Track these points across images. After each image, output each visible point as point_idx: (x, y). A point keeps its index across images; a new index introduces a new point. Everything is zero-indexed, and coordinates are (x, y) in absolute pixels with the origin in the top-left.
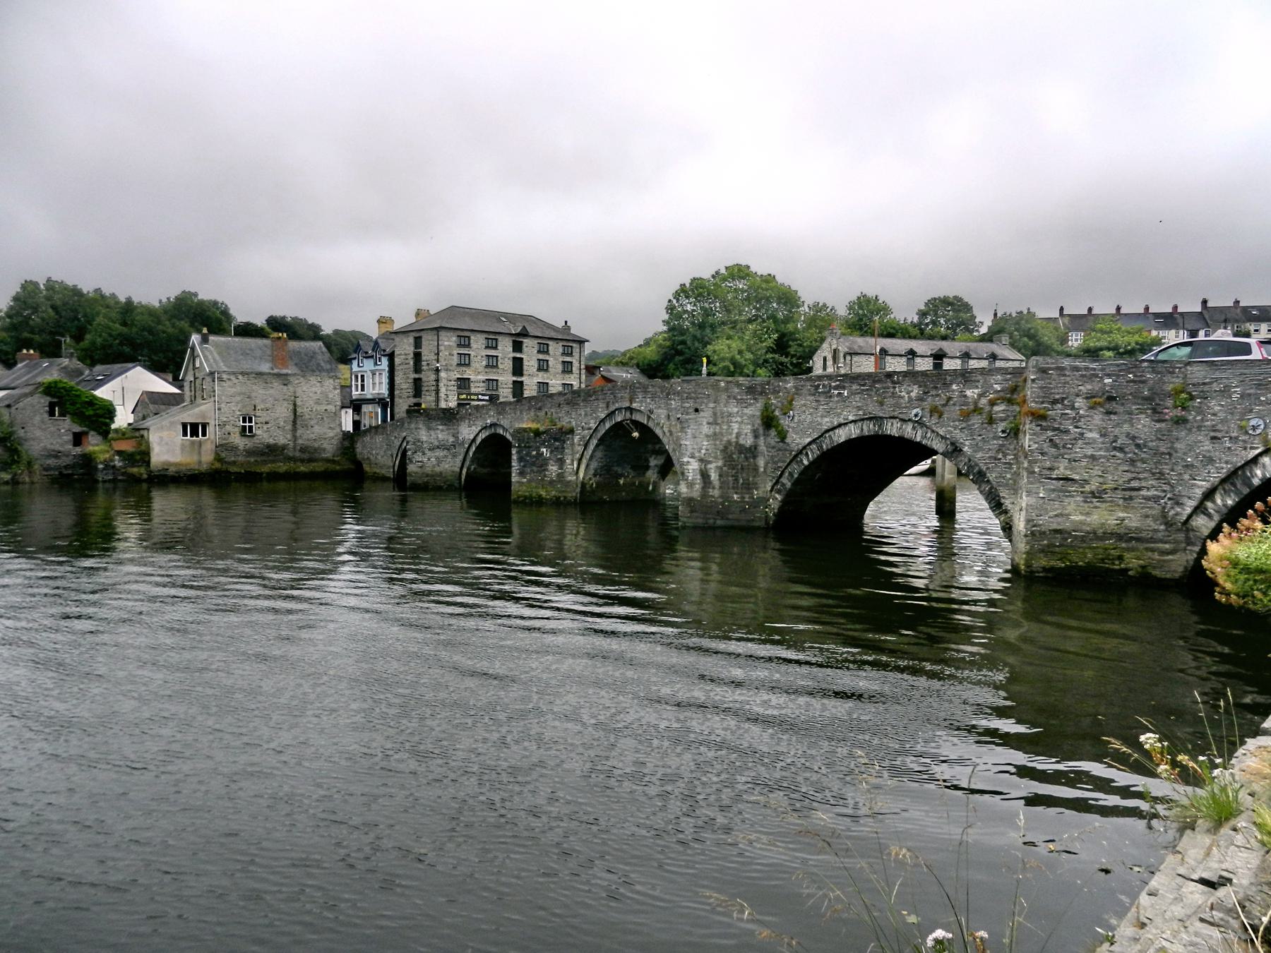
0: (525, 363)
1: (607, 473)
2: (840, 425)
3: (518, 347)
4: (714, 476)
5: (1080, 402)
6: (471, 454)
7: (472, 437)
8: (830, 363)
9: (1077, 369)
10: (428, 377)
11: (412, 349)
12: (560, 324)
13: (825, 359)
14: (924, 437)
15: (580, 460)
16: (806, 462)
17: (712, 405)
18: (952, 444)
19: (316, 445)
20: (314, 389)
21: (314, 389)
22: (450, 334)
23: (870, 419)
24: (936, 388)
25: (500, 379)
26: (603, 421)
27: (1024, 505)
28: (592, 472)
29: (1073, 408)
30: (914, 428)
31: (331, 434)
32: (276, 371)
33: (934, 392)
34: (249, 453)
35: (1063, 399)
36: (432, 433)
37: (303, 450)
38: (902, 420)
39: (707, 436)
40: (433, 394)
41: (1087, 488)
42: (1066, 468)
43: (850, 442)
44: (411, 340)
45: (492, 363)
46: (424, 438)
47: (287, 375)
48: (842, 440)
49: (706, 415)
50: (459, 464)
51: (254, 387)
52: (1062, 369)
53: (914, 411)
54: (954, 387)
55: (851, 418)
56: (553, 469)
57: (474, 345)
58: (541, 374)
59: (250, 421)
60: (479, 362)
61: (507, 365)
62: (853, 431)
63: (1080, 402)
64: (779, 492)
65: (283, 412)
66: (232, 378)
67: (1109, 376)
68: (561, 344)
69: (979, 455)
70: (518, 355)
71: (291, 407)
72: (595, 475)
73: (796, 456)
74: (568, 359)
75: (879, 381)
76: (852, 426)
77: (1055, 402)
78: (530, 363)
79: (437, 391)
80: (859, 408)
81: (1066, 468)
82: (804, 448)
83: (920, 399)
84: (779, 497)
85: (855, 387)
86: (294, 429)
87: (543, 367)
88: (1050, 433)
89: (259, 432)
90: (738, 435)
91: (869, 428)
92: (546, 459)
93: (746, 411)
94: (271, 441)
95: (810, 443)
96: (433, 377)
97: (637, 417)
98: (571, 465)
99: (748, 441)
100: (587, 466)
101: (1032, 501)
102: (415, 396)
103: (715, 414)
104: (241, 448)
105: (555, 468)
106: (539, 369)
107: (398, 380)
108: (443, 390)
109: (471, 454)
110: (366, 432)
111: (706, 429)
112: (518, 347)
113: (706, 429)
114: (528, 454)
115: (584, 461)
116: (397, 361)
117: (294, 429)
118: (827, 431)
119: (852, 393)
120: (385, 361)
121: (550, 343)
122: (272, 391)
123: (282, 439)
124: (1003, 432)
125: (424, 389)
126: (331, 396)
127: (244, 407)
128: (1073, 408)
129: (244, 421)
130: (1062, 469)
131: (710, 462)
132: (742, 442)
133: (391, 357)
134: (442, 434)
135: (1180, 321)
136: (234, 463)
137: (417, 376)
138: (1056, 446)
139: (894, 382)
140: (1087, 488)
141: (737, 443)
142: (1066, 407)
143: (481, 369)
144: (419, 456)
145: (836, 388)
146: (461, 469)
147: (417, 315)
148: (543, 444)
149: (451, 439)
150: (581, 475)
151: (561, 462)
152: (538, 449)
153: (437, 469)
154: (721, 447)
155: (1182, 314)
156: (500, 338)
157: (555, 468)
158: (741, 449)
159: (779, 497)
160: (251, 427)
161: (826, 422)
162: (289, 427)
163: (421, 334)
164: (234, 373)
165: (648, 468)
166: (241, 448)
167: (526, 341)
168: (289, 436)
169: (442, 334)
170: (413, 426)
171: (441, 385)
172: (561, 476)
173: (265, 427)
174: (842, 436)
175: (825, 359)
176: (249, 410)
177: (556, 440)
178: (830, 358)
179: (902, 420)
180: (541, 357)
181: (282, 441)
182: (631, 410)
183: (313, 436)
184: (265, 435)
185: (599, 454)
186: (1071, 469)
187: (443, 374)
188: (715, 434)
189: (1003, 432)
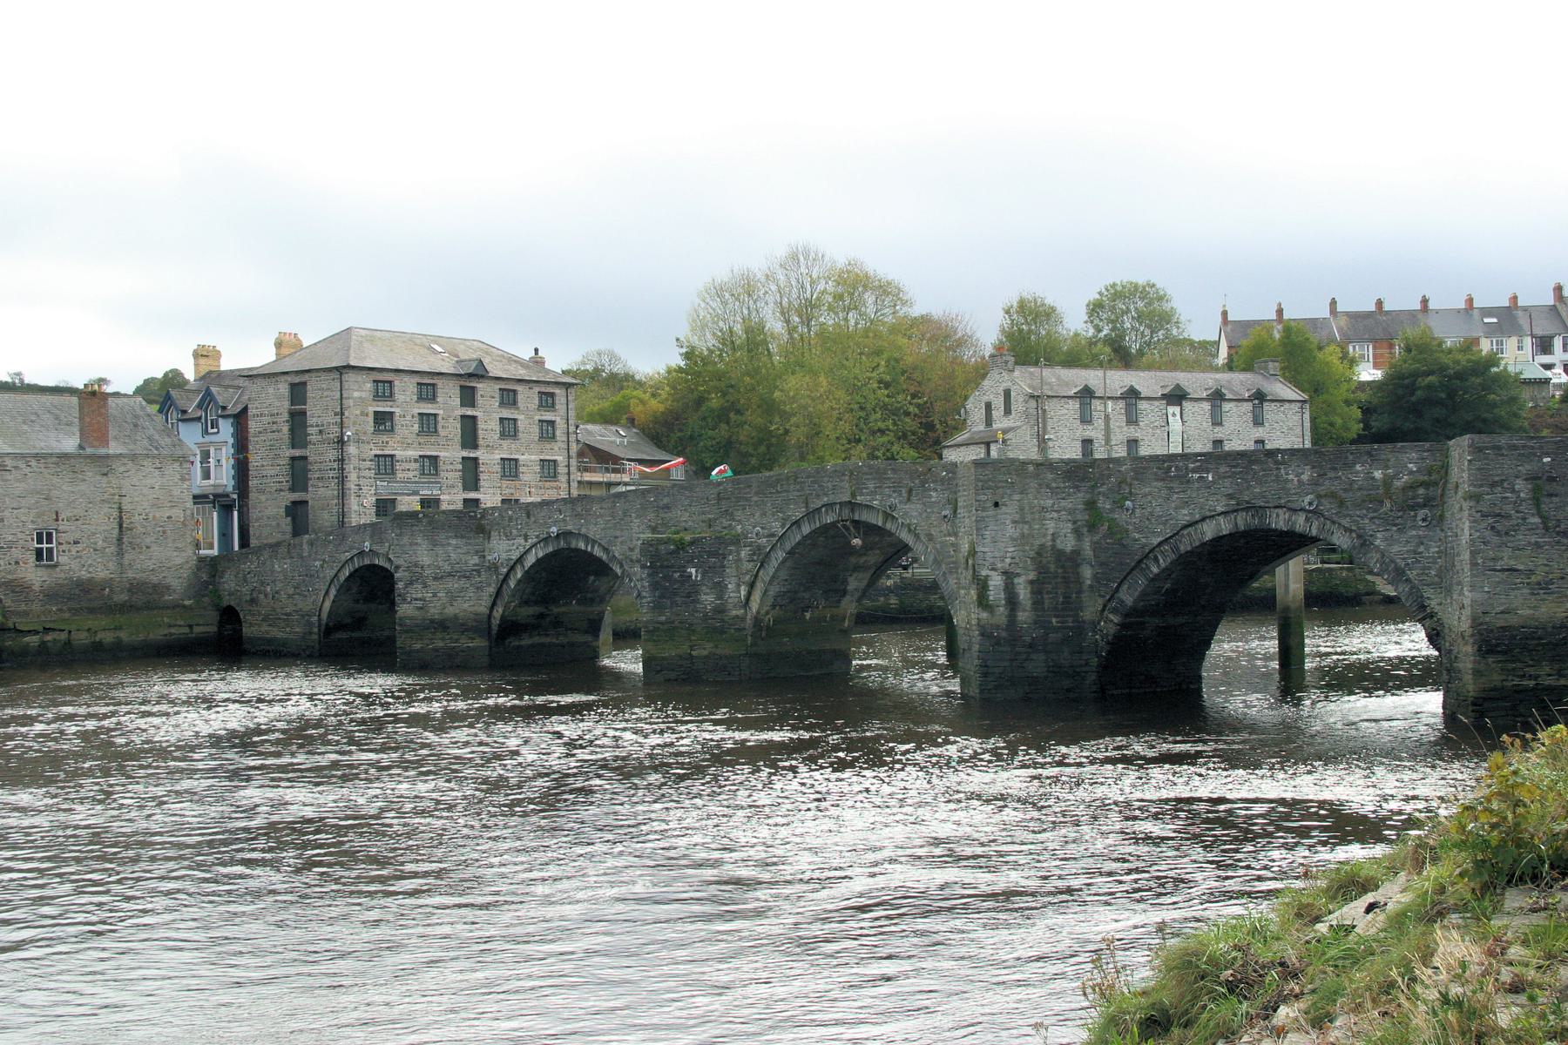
0: (481, 425)
1: (791, 602)
2: (1203, 519)
3: (468, 396)
4: (1023, 593)
5: (1520, 484)
6: (512, 584)
7: (515, 556)
8: (997, 413)
9: (1515, 448)
10: (321, 455)
11: (287, 404)
12: (527, 354)
13: (988, 406)
14: (1321, 529)
15: (752, 586)
16: (1155, 570)
17: (1017, 497)
18: (1359, 537)
19: (155, 580)
20: (149, 482)
21: (149, 482)
22: (406, 378)
23: (1247, 509)
24: (1335, 469)
25: (521, 458)
26: (797, 523)
27: (1467, 602)
28: (770, 601)
29: (1513, 491)
30: (1307, 519)
31: (179, 561)
32: (89, 451)
33: (1331, 474)
34: (51, 595)
35: (1502, 481)
36: (440, 550)
37: (135, 587)
38: (1290, 509)
39: (1013, 539)
40: (333, 484)
41: (1534, 579)
42: (1510, 558)
43: (1218, 540)
44: (284, 389)
45: (428, 424)
46: (425, 559)
47: (107, 456)
48: (1209, 536)
49: (1009, 511)
50: (486, 601)
51: (55, 480)
52: (1499, 448)
53: (1308, 499)
54: (1358, 467)
55: (1220, 509)
56: (708, 599)
57: (399, 397)
58: (506, 443)
59: (49, 541)
60: (406, 425)
61: (451, 428)
62: (1225, 526)
63: (1520, 484)
64: (1114, 611)
65: (101, 522)
66: (21, 464)
67: (1547, 455)
68: (536, 390)
69: (1395, 549)
70: (470, 412)
71: (115, 514)
72: (774, 606)
73: (1140, 561)
74: (548, 416)
75: (1256, 462)
76: (1221, 519)
77: (1494, 485)
78: (488, 426)
79: (342, 480)
80: (1230, 496)
81: (1510, 558)
82: (1152, 551)
83: (1314, 483)
84: (1115, 619)
85: (1223, 469)
86: (120, 553)
87: (509, 429)
88: (1491, 520)
89: (63, 559)
90: (1054, 537)
91: (1243, 521)
92: (695, 584)
93: (1064, 504)
94: (84, 574)
95: (1160, 544)
96: (332, 454)
97: (865, 516)
98: (735, 591)
99: (1068, 544)
100: (765, 593)
101: (1478, 596)
102: (293, 489)
103: (1022, 509)
104: (36, 588)
105: (711, 598)
106: (503, 435)
107: (255, 460)
108: (353, 477)
109: (512, 584)
110: (260, 549)
111: (1011, 531)
112: (468, 396)
113: (1011, 531)
114: (667, 578)
115: (759, 586)
116: (253, 426)
117: (120, 553)
118: (1186, 527)
119: (1220, 477)
120: (226, 430)
121: (519, 388)
122: (83, 487)
123: (100, 568)
124: (1424, 520)
125: (312, 475)
126: (176, 492)
127: (39, 515)
128: (1513, 491)
129: (40, 541)
130: (1507, 561)
131: (1018, 575)
132: (1060, 545)
133: (240, 419)
134: (457, 551)
135: (1523, 321)
136: (26, 614)
137: (297, 453)
138: (1498, 533)
139: (1277, 462)
140: (1534, 579)
141: (1053, 547)
142: (1505, 490)
143: (412, 438)
144: (416, 591)
145: (1194, 471)
146: (492, 608)
147: (279, 345)
148: (690, 562)
149: (476, 560)
150: (755, 605)
151: (720, 588)
152: (682, 569)
153: (450, 611)
154: (1032, 554)
155: (1525, 309)
156: (440, 382)
157: (711, 598)
158: (1059, 554)
159: (1115, 619)
160: (50, 551)
161: (1184, 516)
162: (113, 549)
163: (305, 378)
164: (23, 456)
165: (844, 593)
166: (36, 588)
167: (482, 387)
168: (111, 565)
169: (350, 377)
170: (405, 540)
171: (349, 467)
172: (720, 610)
173: (74, 549)
174: (1209, 531)
175: (988, 406)
176: (47, 523)
177: (711, 554)
178: (998, 403)
179: (1290, 509)
180: (506, 413)
181: (101, 574)
182: (852, 506)
183: (150, 565)
184: (75, 565)
185: (783, 575)
186: (1516, 558)
187: (352, 449)
188: (1023, 536)
189: (1424, 520)
